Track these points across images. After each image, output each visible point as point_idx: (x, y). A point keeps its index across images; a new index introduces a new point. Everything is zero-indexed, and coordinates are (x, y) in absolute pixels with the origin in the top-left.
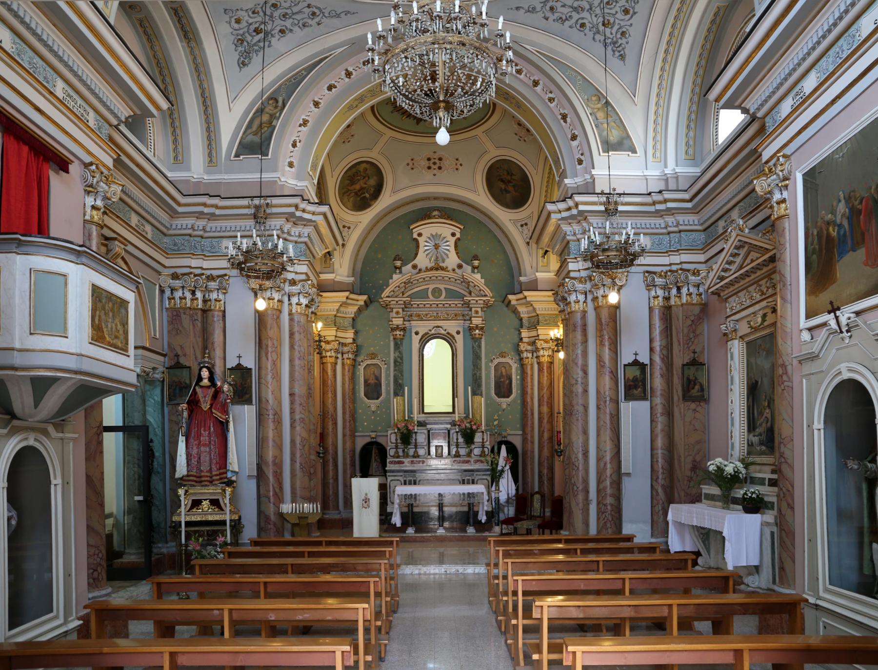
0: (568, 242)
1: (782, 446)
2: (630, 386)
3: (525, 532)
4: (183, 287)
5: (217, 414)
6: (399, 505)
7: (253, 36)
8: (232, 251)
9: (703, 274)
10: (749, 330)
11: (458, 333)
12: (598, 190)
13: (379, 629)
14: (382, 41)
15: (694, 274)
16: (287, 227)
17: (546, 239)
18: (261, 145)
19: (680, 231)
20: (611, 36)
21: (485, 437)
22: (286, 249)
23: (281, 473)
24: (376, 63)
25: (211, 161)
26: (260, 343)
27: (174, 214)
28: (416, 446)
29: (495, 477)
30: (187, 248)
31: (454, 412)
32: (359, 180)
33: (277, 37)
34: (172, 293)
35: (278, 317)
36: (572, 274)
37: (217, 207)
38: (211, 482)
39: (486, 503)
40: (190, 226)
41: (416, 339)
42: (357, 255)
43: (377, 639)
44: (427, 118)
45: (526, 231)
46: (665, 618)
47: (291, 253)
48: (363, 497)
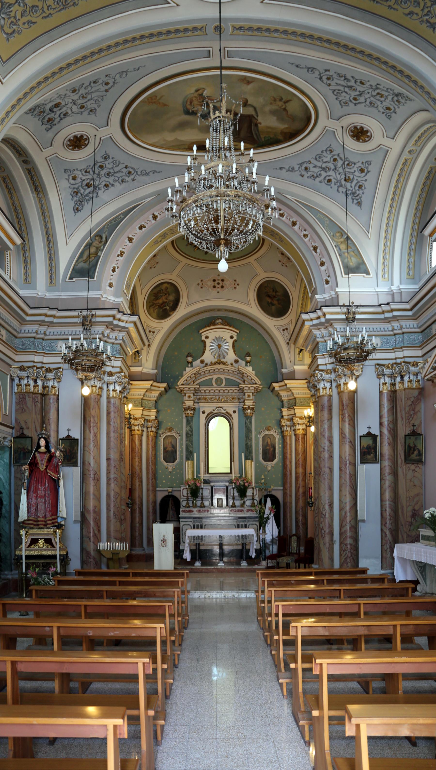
0: (318, 343)
2: (365, 452)
3: (285, 565)
4: (28, 377)
5: (51, 473)
6: (189, 544)
7: (85, 189)
8: (64, 351)
9: (421, 365)
11: (234, 412)
12: (341, 303)
13: (173, 642)
14: (179, 195)
15: (413, 365)
16: (107, 332)
17: (301, 340)
18: (89, 270)
19: (403, 333)
20: (351, 189)
21: (255, 492)
22: (105, 348)
23: (100, 519)
24: (174, 210)
25: (51, 282)
26: (85, 420)
27: (23, 322)
28: (202, 499)
29: (262, 522)
30: (32, 348)
31: (231, 473)
32: (161, 296)
33: (103, 189)
34: (20, 381)
35: (99, 400)
36: (321, 367)
37: (54, 317)
38: (45, 525)
39: (255, 543)
40: (34, 331)
41: (203, 417)
42: (159, 353)
43: (172, 650)
44: (211, 252)
45: (286, 334)
46: (391, 635)
47: (109, 352)
48: (162, 538)
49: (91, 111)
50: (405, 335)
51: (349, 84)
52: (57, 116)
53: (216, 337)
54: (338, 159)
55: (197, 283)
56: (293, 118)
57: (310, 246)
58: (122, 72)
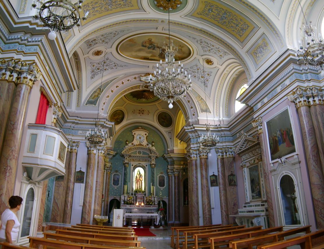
0: (190, 139)
1: (268, 194)
7: (96, 70)
10: (250, 165)
11: (147, 166)
19: (225, 136)
25: (78, 105)
32: (117, 116)
36: (192, 148)
37: (79, 120)
40: (70, 126)
49: (106, 43)
50: (226, 137)
51: (208, 45)
52: (93, 44)
53: (139, 134)
54: (199, 69)
55: (132, 111)
56: (184, 53)
57: (187, 100)
58: (122, 31)
